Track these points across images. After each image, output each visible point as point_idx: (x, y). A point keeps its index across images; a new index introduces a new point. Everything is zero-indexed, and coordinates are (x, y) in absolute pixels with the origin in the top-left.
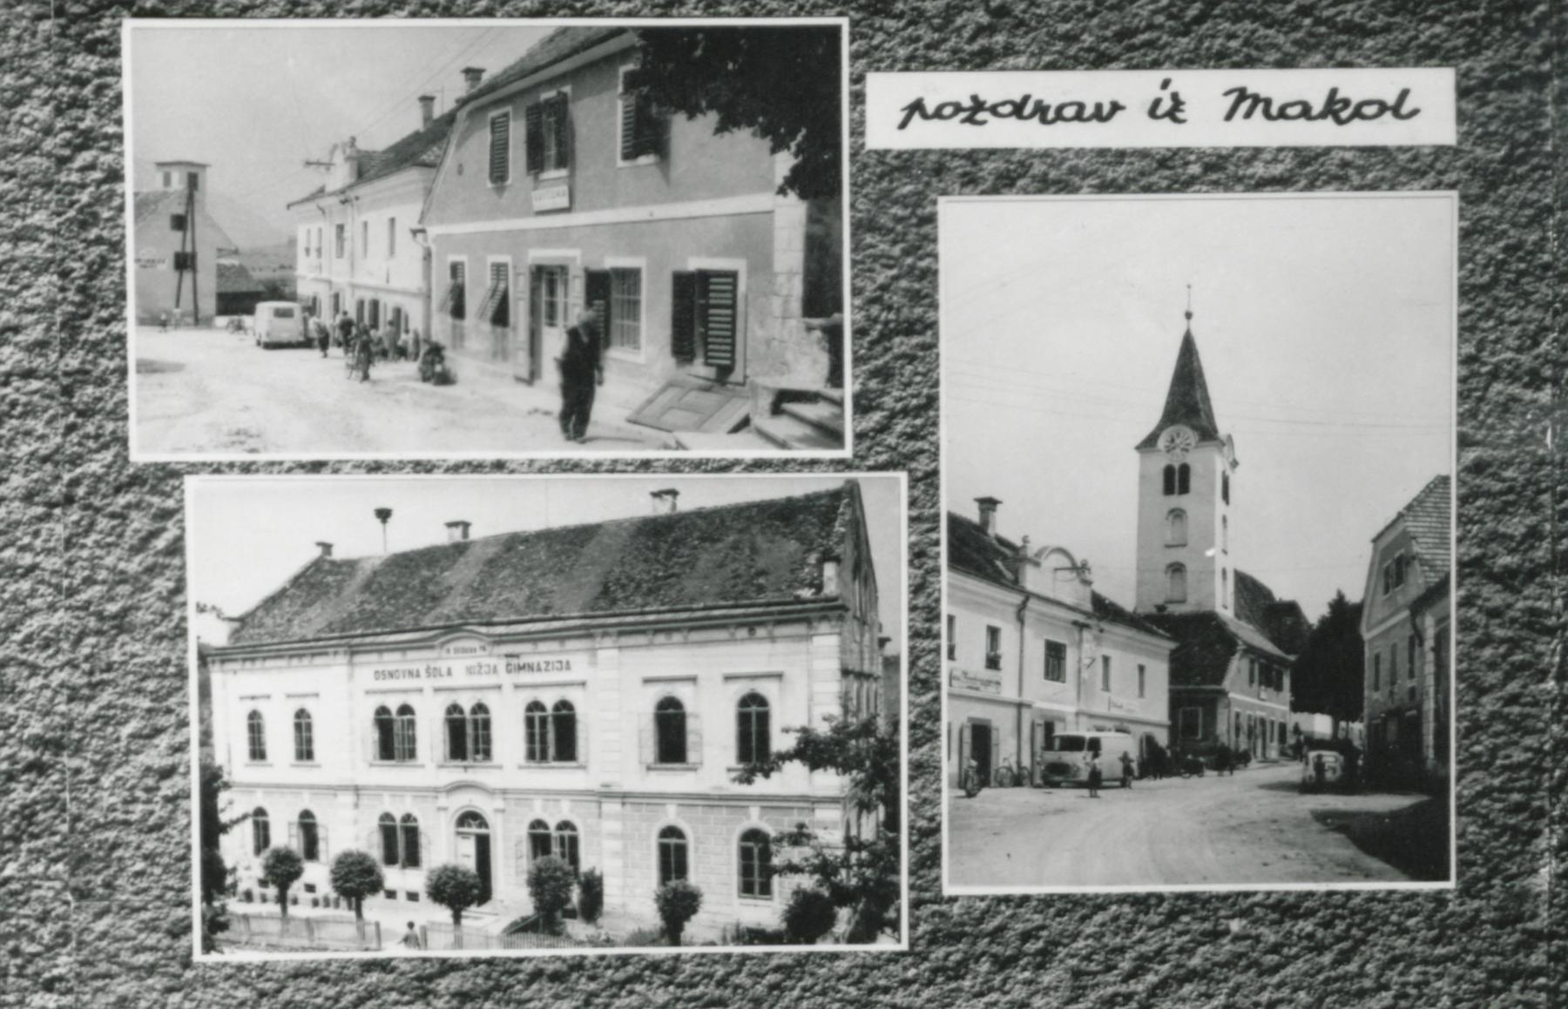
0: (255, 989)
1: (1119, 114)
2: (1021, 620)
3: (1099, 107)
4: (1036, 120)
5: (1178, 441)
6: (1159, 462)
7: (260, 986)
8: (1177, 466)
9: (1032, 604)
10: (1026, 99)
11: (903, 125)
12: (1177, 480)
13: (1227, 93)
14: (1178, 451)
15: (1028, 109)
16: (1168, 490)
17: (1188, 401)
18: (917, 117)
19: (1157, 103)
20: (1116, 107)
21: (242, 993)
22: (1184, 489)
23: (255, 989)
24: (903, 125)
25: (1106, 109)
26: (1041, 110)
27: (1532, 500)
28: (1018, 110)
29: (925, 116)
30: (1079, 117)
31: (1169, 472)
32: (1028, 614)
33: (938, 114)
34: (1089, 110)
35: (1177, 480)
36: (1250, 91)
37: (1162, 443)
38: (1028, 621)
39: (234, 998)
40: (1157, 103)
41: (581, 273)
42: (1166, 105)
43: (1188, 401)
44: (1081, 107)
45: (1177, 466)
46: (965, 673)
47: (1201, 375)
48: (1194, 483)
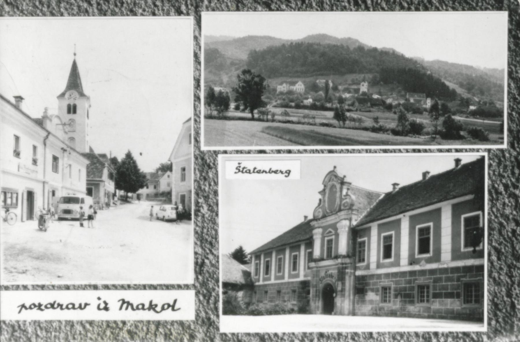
0: (106, 329)
1: (87, 307)
2: (45, 144)
3: (80, 305)
4: (59, 308)
5: (72, 96)
6: (65, 103)
7: (105, 327)
8: (72, 104)
9: (51, 137)
10: (55, 302)
11: (20, 312)
12: (72, 109)
13: (119, 301)
14: (72, 99)
15: (56, 306)
16: (69, 112)
17: (74, 82)
18: (23, 309)
19: (99, 305)
20: (86, 305)
21: (108, 333)
22: (75, 112)
23: (106, 329)
24: (20, 312)
25: (83, 306)
26: (60, 306)
27: (70, 125)
28: (52, 306)
29: (26, 308)
30: (74, 308)
31: (69, 107)
32: (48, 142)
33: (30, 308)
34: (77, 306)
35: (72, 109)
36: (126, 300)
37: (67, 96)
38: (47, 145)
39: (110, 336)
40: (99, 305)
41: (35, 218)
42: (102, 306)
43: (74, 82)
44: (73, 305)
45: (72, 104)
46: (25, 166)
47: (79, 75)
48: (78, 111)
